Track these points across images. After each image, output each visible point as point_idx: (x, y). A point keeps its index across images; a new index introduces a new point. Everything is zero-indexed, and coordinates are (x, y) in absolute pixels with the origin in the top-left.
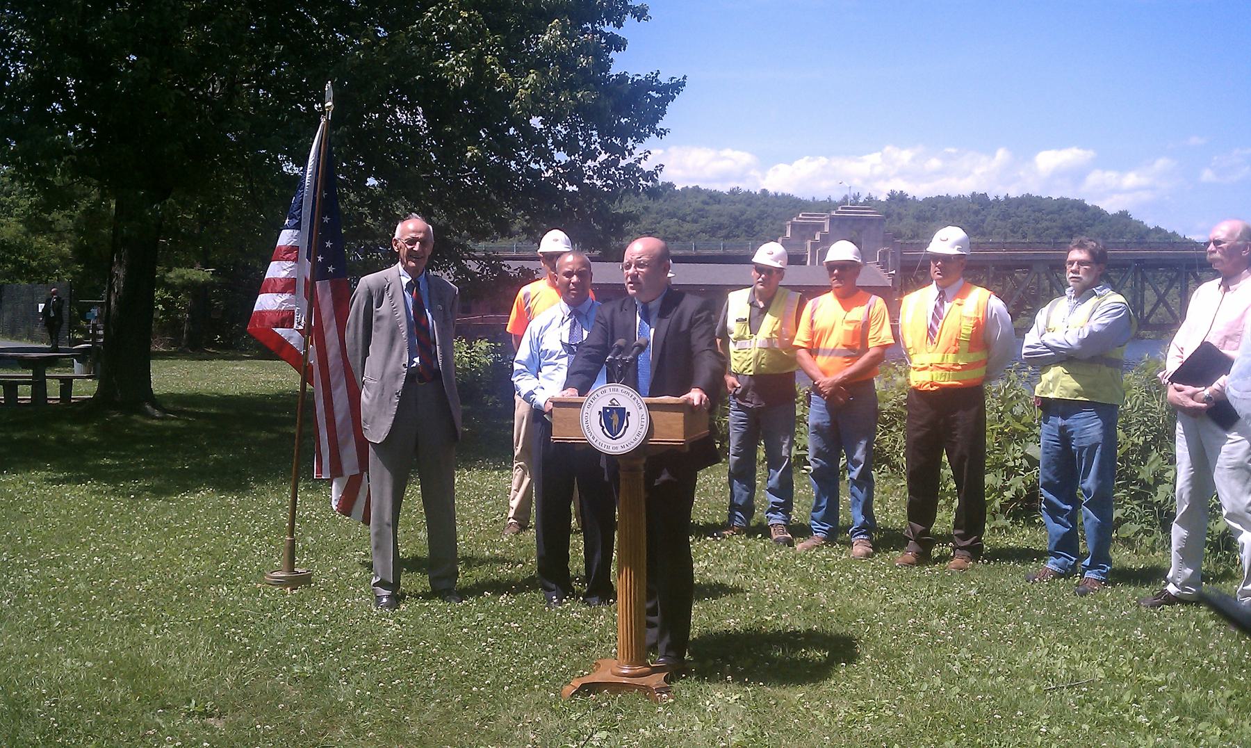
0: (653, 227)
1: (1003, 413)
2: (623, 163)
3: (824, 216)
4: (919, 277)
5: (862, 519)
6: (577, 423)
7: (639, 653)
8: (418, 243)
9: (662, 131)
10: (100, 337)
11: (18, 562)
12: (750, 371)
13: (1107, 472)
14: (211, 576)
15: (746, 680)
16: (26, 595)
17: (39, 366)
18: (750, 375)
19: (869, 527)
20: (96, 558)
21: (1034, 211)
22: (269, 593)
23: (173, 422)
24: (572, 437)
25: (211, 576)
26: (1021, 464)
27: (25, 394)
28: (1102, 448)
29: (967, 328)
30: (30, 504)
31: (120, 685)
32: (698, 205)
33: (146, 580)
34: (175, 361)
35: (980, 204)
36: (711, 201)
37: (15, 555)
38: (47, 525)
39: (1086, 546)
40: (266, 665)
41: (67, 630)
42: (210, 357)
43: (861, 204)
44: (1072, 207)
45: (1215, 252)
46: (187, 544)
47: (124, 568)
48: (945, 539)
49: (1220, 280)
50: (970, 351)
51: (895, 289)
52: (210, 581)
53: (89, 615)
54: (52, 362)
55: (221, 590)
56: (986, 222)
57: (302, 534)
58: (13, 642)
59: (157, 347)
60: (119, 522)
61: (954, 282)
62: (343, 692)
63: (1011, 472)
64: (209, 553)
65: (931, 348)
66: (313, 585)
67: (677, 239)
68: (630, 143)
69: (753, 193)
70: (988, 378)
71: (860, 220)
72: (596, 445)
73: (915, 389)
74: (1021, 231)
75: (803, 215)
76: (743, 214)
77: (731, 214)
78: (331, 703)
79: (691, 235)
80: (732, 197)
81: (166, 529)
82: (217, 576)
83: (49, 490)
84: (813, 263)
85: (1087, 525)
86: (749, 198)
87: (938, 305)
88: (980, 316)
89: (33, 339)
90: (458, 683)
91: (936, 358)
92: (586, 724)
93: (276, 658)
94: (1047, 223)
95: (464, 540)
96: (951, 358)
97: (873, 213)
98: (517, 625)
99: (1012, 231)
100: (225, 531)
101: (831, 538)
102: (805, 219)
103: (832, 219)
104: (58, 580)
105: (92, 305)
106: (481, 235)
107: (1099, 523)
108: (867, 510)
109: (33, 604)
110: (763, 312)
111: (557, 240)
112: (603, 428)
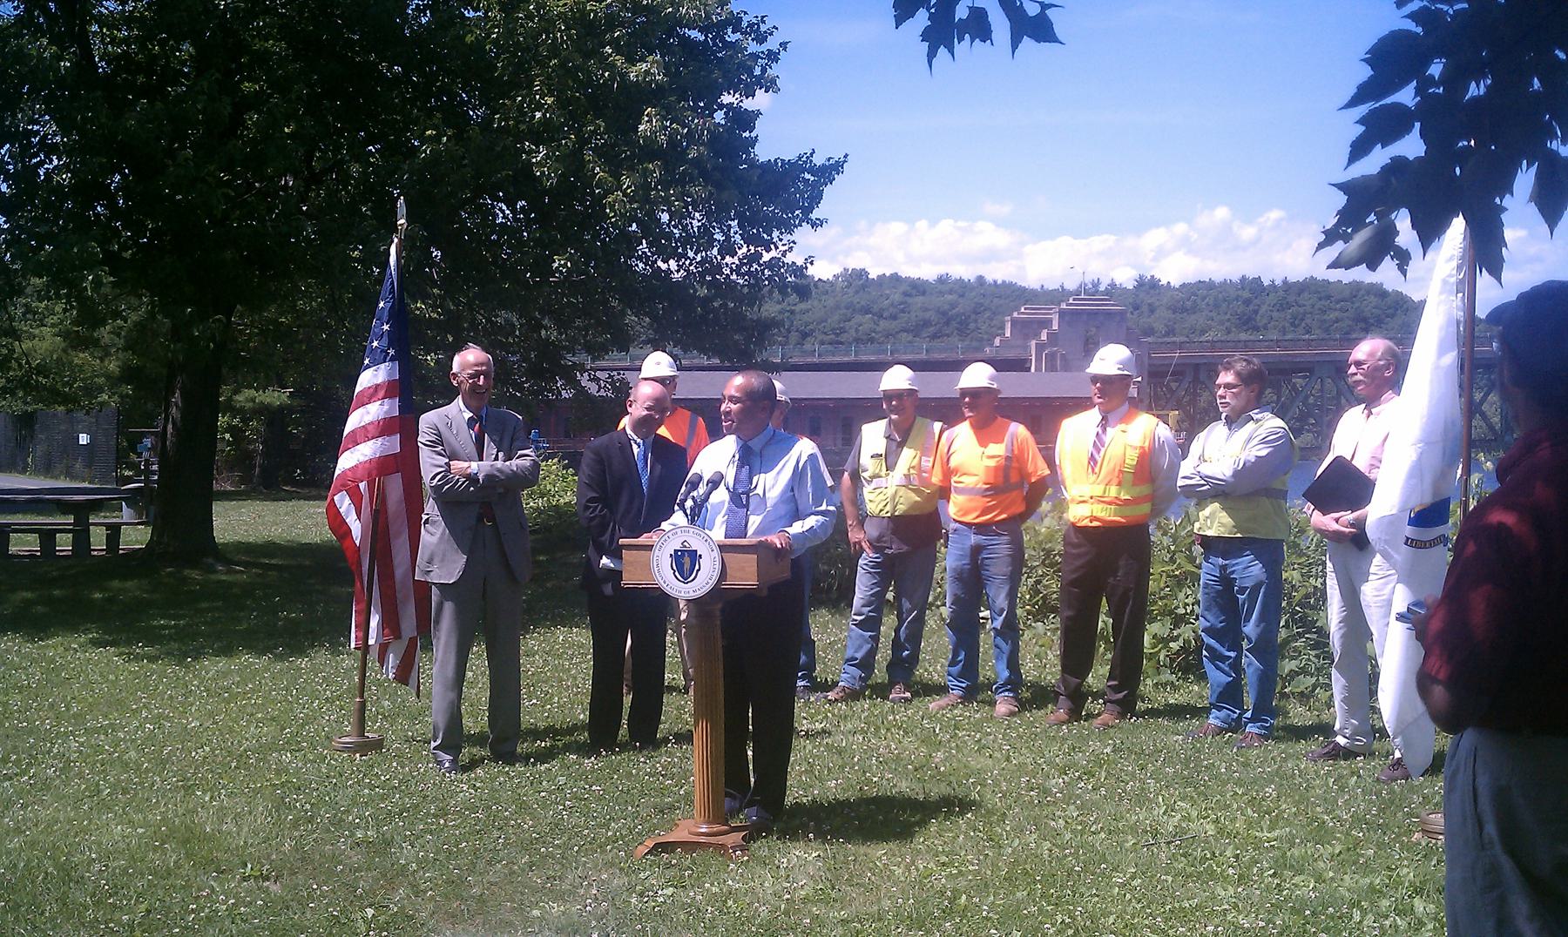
0: (841, 325)
1: (1174, 553)
2: (766, 257)
3: (1051, 309)
4: (1171, 384)
5: (1007, 674)
6: (647, 567)
7: (718, 815)
8: (482, 377)
9: (818, 222)
10: (154, 473)
11: (62, 729)
12: (887, 512)
13: (1270, 618)
14: (274, 743)
15: (829, 837)
16: (72, 764)
17: (82, 511)
18: (889, 517)
19: (1014, 682)
20: (148, 725)
21: (1320, 299)
22: (336, 760)
23: (238, 576)
24: (643, 582)
25: (274, 743)
26: (1193, 611)
27: (64, 543)
28: (1266, 589)
29: (1132, 458)
30: (73, 669)
31: (173, 851)
32: (897, 297)
33: (203, 747)
34: (246, 503)
35: (1252, 291)
36: (914, 292)
37: (59, 723)
38: (93, 691)
39: (1249, 700)
40: (328, 831)
41: (116, 798)
42: (289, 497)
43: (1103, 293)
44: (1368, 293)
45: (1356, 374)
46: (249, 710)
47: (179, 735)
48: (1096, 696)
49: (1364, 405)
50: (1134, 484)
51: (1141, 401)
52: (273, 747)
53: (141, 783)
54: (96, 506)
55: (284, 757)
56: (1260, 312)
57: (378, 699)
58: (59, 811)
59: (222, 485)
60: (174, 687)
61: (1118, 406)
62: (406, 854)
63: (1179, 621)
64: (273, 719)
65: (1093, 478)
66: (384, 750)
67: (872, 340)
68: (776, 234)
69: (966, 280)
70: (1156, 512)
71: (1096, 314)
72: (668, 590)
73: (1073, 524)
74: (1303, 325)
75: (1025, 309)
76: (953, 306)
77: (939, 308)
78: (393, 865)
79: (888, 335)
80: (940, 287)
81: (226, 695)
82: (281, 742)
83: (96, 654)
84: (1038, 369)
85: (1250, 671)
86: (962, 287)
87: (1100, 432)
88: (1147, 444)
89: (73, 478)
90: (527, 846)
91: (1098, 490)
92: (654, 882)
93: (338, 823)
94: (1337, 314)
95: (558, 702)
96: (1113, 491)
97: (1113, 305)
98: (598, 788)
99: (1292, 324)
100: (292, 696)
101: (969, 695)
102: (1077, 305)
103: (1062, 313)
104: (107, 747)
105: (143, 435)
106: (598, 351)
107: (1261, 670)
108: (1013, 664)
109: (80, 773)
110: (901, 445)
111: (658, 364)
112: (675, 571)
